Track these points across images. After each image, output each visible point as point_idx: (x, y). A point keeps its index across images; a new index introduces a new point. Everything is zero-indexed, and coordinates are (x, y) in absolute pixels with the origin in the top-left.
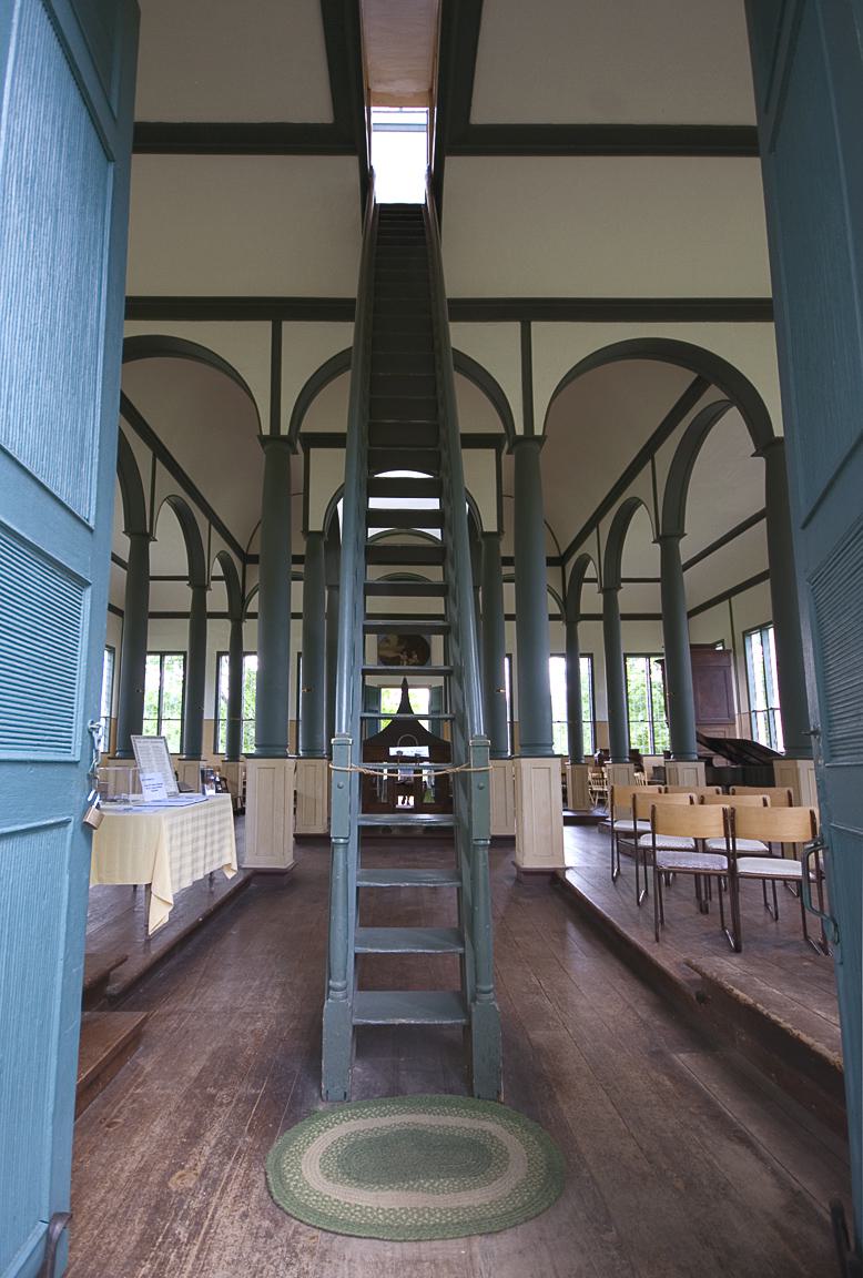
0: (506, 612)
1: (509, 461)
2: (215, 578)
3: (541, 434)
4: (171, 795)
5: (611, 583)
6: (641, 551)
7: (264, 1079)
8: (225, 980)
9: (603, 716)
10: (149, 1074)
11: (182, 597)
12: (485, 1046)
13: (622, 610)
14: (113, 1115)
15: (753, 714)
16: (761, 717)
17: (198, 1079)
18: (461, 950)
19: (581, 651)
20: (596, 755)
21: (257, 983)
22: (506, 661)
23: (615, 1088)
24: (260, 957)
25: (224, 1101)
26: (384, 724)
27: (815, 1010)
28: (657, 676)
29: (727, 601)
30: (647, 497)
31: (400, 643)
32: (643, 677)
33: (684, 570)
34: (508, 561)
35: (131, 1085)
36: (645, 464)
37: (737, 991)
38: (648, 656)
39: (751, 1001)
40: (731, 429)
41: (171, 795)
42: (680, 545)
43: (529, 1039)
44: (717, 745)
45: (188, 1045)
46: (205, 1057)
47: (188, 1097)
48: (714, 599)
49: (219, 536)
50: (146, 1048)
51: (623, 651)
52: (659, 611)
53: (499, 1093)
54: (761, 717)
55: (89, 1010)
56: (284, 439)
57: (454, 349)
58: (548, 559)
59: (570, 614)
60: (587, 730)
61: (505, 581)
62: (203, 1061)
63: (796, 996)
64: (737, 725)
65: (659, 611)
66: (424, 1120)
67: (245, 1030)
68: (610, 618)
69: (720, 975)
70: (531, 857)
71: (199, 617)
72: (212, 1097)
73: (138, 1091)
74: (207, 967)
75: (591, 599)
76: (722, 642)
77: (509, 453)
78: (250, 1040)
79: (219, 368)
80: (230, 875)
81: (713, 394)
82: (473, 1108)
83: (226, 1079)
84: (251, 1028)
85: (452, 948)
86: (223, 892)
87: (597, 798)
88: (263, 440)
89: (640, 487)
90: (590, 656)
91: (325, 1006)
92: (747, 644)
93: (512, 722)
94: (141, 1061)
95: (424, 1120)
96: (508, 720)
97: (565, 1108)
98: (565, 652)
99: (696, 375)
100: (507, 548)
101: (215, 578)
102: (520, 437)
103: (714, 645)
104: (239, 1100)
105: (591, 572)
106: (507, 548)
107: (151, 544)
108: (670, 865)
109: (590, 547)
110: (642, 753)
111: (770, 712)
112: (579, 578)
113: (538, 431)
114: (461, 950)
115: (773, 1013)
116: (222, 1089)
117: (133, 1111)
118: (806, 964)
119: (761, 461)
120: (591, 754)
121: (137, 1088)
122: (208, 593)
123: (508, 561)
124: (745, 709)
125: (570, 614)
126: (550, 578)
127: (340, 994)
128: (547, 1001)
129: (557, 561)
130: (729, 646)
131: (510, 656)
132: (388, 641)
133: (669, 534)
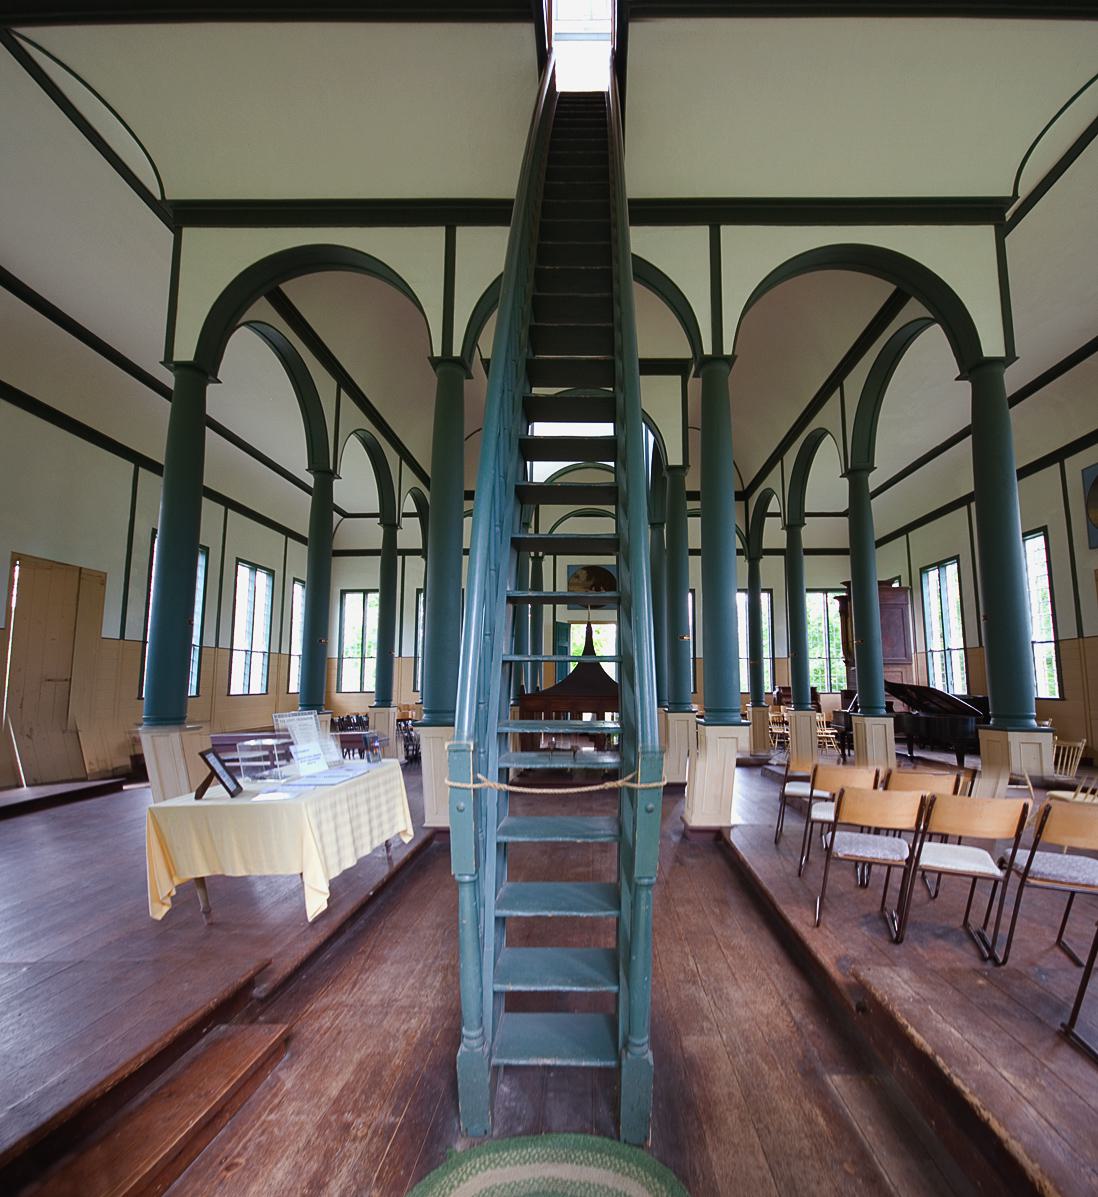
0: (690, 547)
1: (695, 384)
2: (406, 515)
3: (730, 353)
4: (331, 765)
5: (795, 521)
6: (827, 484)
7: (406, 1102)
8: (389, 963)
9: (783, 652)
10: (288, 1092)
11: (372, 534)
12: (637, 1091)
13: (805, 545)
14: (236, 1152)
15: (929, 654)
16: (937, 658)
17: (337, 1100)
18: (614, 989)
19: (762, 586)
20: (775, 693)
21: (420, 966)
22: (690, 596)
23: (767, 1127)
24: (428, 932)
25: (359, 1134)
26: (572, 666)
27: (1001, 1070)
28: (835, 607)
29: (905, 536)
30: (834, 425)
31: (588, 579)
32: (822, 612)
33: (872, 498)
34: (693, 496)
35: (265, 1109)
36: (834, 391)
37: (911, 1030)
38: (826, 591)
39: (929, 1049)
40: (932, 349)
41: (331, 765)
42: (869, 479)
43: (681, 1047)
44: (895, 689)
45: (336, 1050)
46: (351, 1068)
47: (321, 1127)
48: (891, 534)
49: (409, 470)
50: (292, 1056)
51: (805, 588)
52: (847, 545)
53: (646, 1139)
54: (937, 658)
55: (226, 1022)
56: (456, 361)
57: (633, 255)
58: (736, 493)
59: (754, 551)
60: (767, 666)
61: (689, 516)
62: (347, 1075)
63: (980, 1044)
64: (913, 665)
65: (847, 545)
66: (566, 1172)
67: (398, 1031)
68: (793, 555)
69: (892, 1000)
70: (700, 814)
71: (390, 554)
72: (347, 1127)
73: (270, 1118)
74: (374, 947)
75: (774, 534)
76: (899, 578)
77: (696, 375)
78: (401, 1045)
79: (391, 282)
80: (407, 840)
81: (914, 309)
82: (619, 1155)
83: (366, 1101)
84: (404, 1027)
85: (604, 985)
86: (399, 856)
87: (777, 740)
88: (435, 362)
89: (828, 416)
90: (770, 591)
91: (459, 1054)
92: (924, 581)
93: (694, 658)
94: (282, 1075)
95: (566, 1172)
96: (692, 656)
97: (714, 1158)
98: (747, 587)
99: (893, 287)
100: (692, 482)
101: (406, 515)
102: (708, 356)
103: (892, 581)
104: (375, 1132)
105: (774, 506)
106: (692, 482)
107: (335, 482)
108: (847, 852)
109: (773, 481)
110: (819, 691)
111: (947, 652)
112: (762, 512)
113: (728, 350)
114: (614, 989)
115: (957, 1076)
116: (359, 1116)
117: (259, 1146)
118: (981, 982)
119: (967, 385)
120: (769, 691)
121: (271, 1111)
122: (399, 532)
123: (693, 496)
124: (921, 648)
125: (754, 551)
126: (735, 517)
127: (475, 1043)
128: (702, 994)
129: (743, 496)
130: (905, 584)
131: (693, 591)
132: (578, 577)
133: (857, 469)
